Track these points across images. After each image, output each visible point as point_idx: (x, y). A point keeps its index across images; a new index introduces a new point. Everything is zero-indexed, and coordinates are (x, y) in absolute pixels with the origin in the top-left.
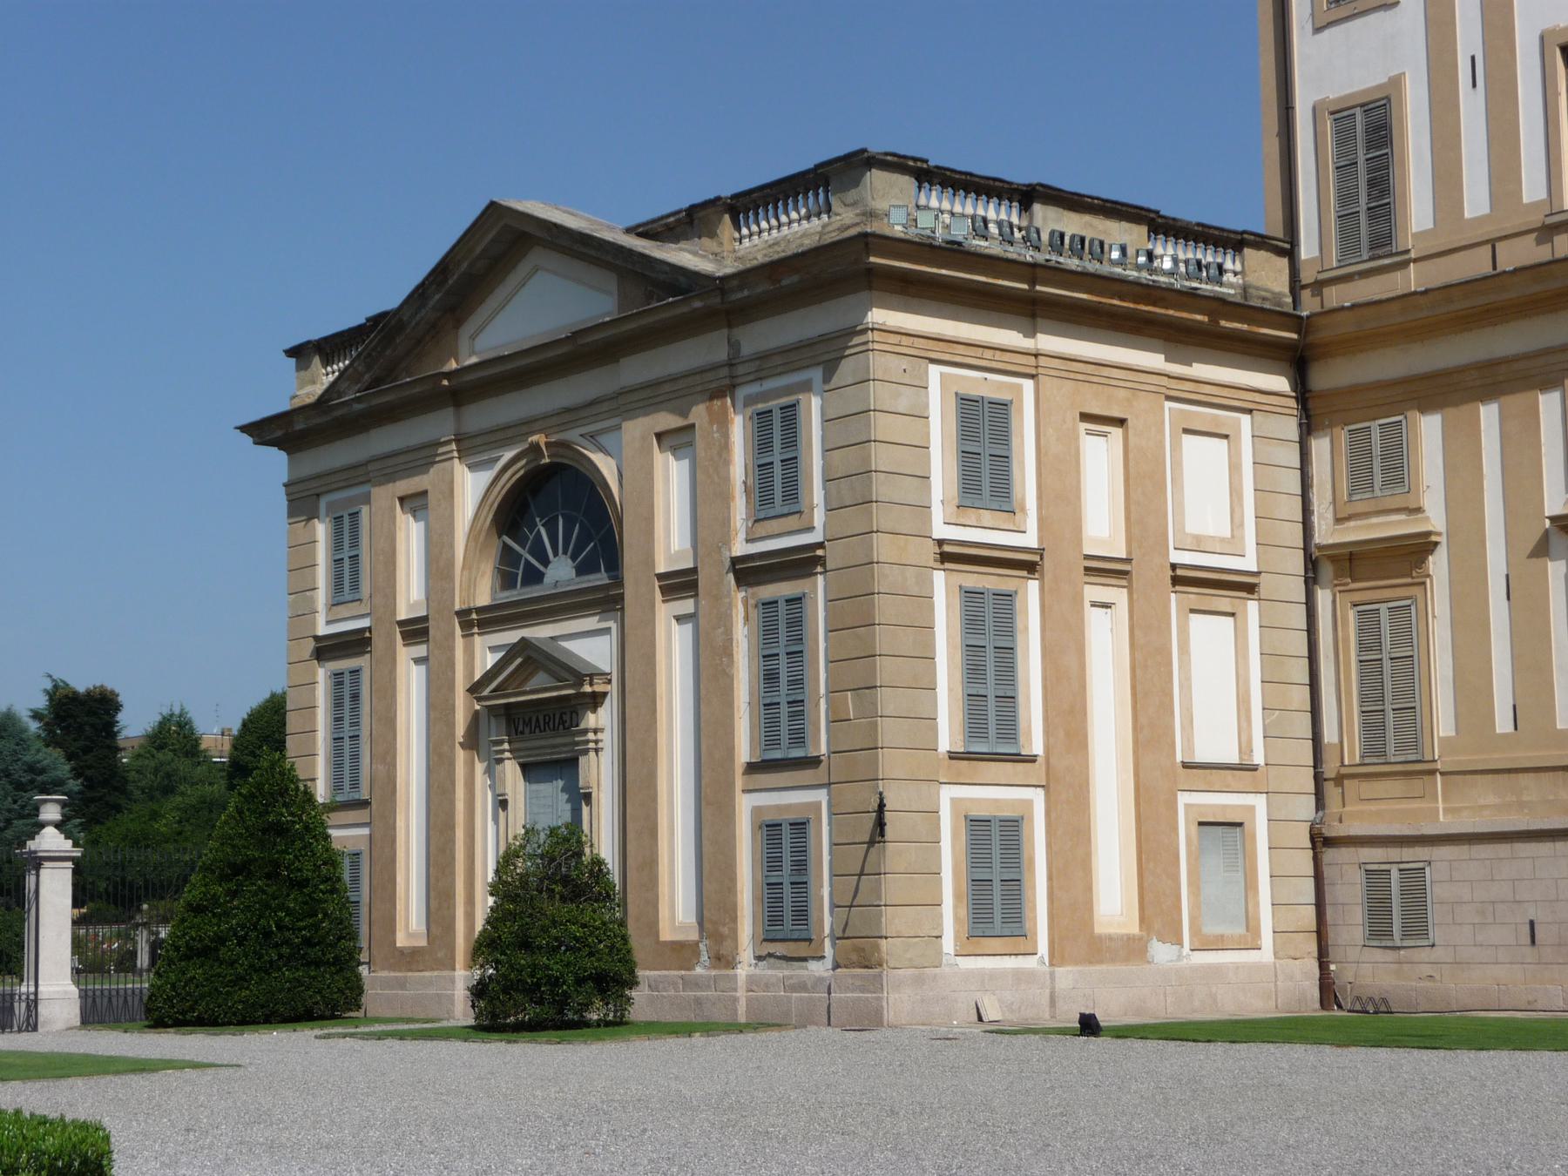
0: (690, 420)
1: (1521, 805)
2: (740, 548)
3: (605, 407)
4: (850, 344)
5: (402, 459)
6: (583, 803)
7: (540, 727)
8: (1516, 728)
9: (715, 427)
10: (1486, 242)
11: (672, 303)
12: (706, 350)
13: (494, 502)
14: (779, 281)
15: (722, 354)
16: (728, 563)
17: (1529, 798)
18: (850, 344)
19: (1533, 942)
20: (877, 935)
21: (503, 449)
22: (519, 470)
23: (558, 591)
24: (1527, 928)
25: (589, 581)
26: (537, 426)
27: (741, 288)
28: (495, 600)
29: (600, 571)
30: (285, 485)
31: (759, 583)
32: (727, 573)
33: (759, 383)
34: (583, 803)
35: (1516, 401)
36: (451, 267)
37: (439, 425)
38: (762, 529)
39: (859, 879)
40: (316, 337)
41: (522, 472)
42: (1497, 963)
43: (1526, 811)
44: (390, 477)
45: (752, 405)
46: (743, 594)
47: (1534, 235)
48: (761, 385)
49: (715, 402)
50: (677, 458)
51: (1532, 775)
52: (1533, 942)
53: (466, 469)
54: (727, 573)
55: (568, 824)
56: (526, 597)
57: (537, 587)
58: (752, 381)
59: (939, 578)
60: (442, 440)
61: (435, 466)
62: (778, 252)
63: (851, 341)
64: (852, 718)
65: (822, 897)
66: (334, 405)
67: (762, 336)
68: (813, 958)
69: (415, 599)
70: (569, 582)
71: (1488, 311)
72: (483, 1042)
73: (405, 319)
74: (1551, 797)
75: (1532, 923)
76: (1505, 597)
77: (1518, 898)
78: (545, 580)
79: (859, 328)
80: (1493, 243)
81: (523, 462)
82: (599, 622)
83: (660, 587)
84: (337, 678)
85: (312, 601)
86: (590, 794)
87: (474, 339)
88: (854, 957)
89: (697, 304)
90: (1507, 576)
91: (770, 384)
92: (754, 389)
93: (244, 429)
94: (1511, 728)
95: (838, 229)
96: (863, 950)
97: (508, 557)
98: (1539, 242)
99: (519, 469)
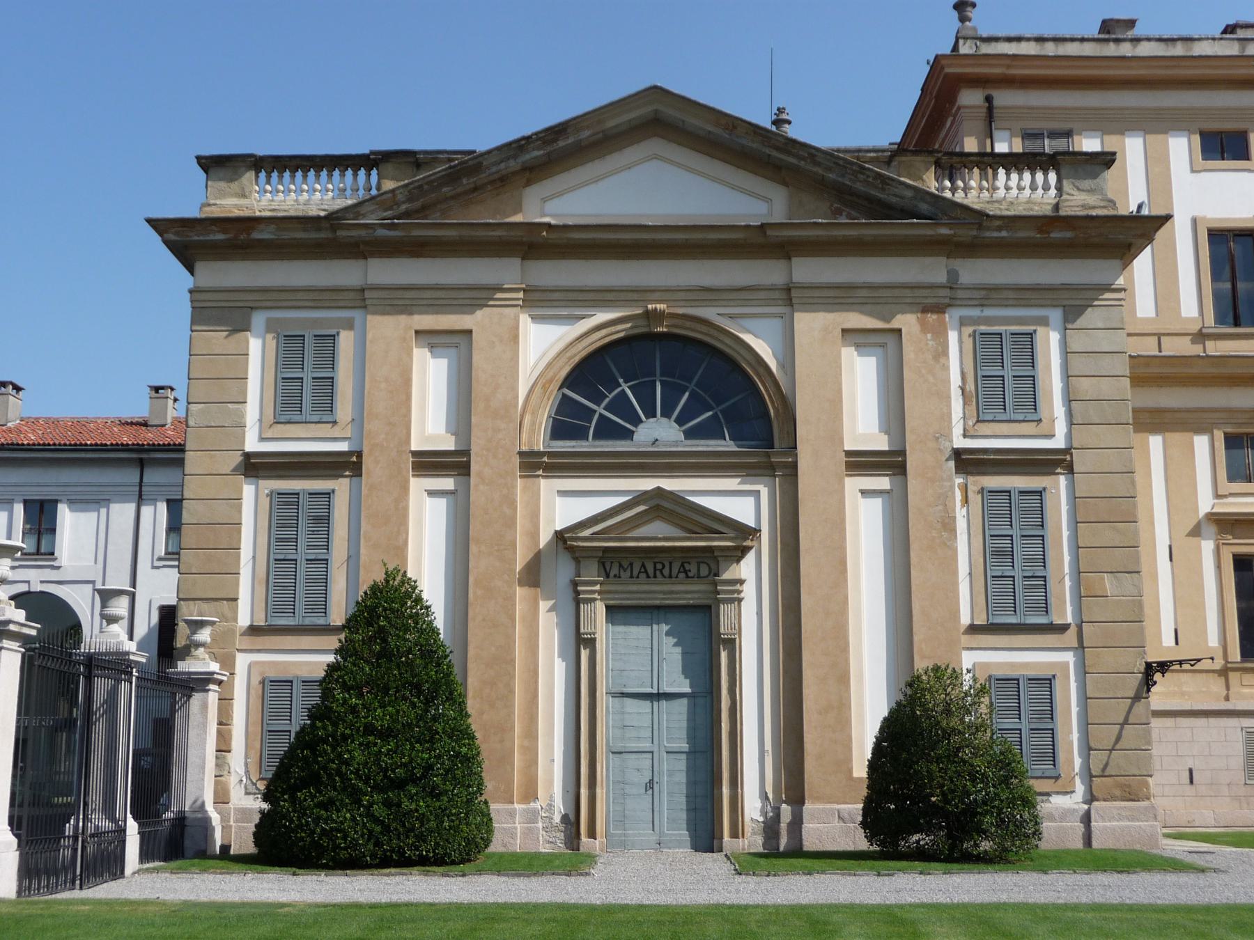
0: (895, 324)
1: (1183, 694)
2: (960, 442)
3: (762, 295)
4: (1101, 297)
5: (428, 294)
6: (582, 647)
7: (646, 572)
8: (1177, 643)
9: (929, 336)
10: (1154, 334)
11: (863, 223)
12: (932, 270)
13: (575, 355)
14: (1049, 233)
15: (941, 277)
16: (948, 453)
17: (1187, 689)
18: (1101, 297)
19: (1191, 782)
20: (1145, 773)
21: (595, 309)
22: (622, 331)
23: (656, 449)
24: (1187, 773)
25: (708, 446)
26: (656, 296)
27: (999, 229)
28: (549, 446)
29: (587, 439)
30: (191, 292)
31: (984, 474)
32: (947, 460)
33: (981, 308)
34: (582, 647)
35: (1176, 437)
36: (569, 130)
37: (506, 271)
38: (984, 429)
39: (1121, 730)
40: (261, 154)
41: (622, 335)
42: (1163, 796)
43: (1186, 697)
44: (407, 309)
45: (974, 325)
46: (961, 480)
47: (1190, 337)
48: (982, 311)
49: (929, 315)
50: (434, 356)
51: (1190, 674)
52: (1191, 782)
53: (529, 319)
54: (947, 460)
55: (939, 667)
56: (607, 450)
57: (628, 442)
58: (976, 306)
59: (248, 491)
60: (505, 286)
61: (485, 309)
62: (1000, 209)
63: (1102, 295)
64: (1109, 595)
65: (1072, 742)
66: (344, 224)
67: (974, 272)
68: (1058, 793)
69: (430, 432)
70: (676, 443)
71: (1161, 377)
72: (879, 875)
73: (485, 163)
74: (1204, 689)
75: (1191, 771)
76: (1168, 559)
77: (1180, 754)
78: (635, 437)
79: (1113, 287)
80: (1159, 336)
81: (629, 325)
82: (739, 484)
83: (413, 462)
84: (286, 500)
85: (242, 415)
86: (594, 640)
87: (544, 202)
88: (1118, 793)
89: (944, 231)
90: (1170, 547)
91: (990, 312)
92: (975, 312)
93: (151, 222)
94: (1173, 643)
95: (1082, 206)
96: (1129, 786)
97: (565, 405)
98: (1193, 342)
99: (620, 331)
